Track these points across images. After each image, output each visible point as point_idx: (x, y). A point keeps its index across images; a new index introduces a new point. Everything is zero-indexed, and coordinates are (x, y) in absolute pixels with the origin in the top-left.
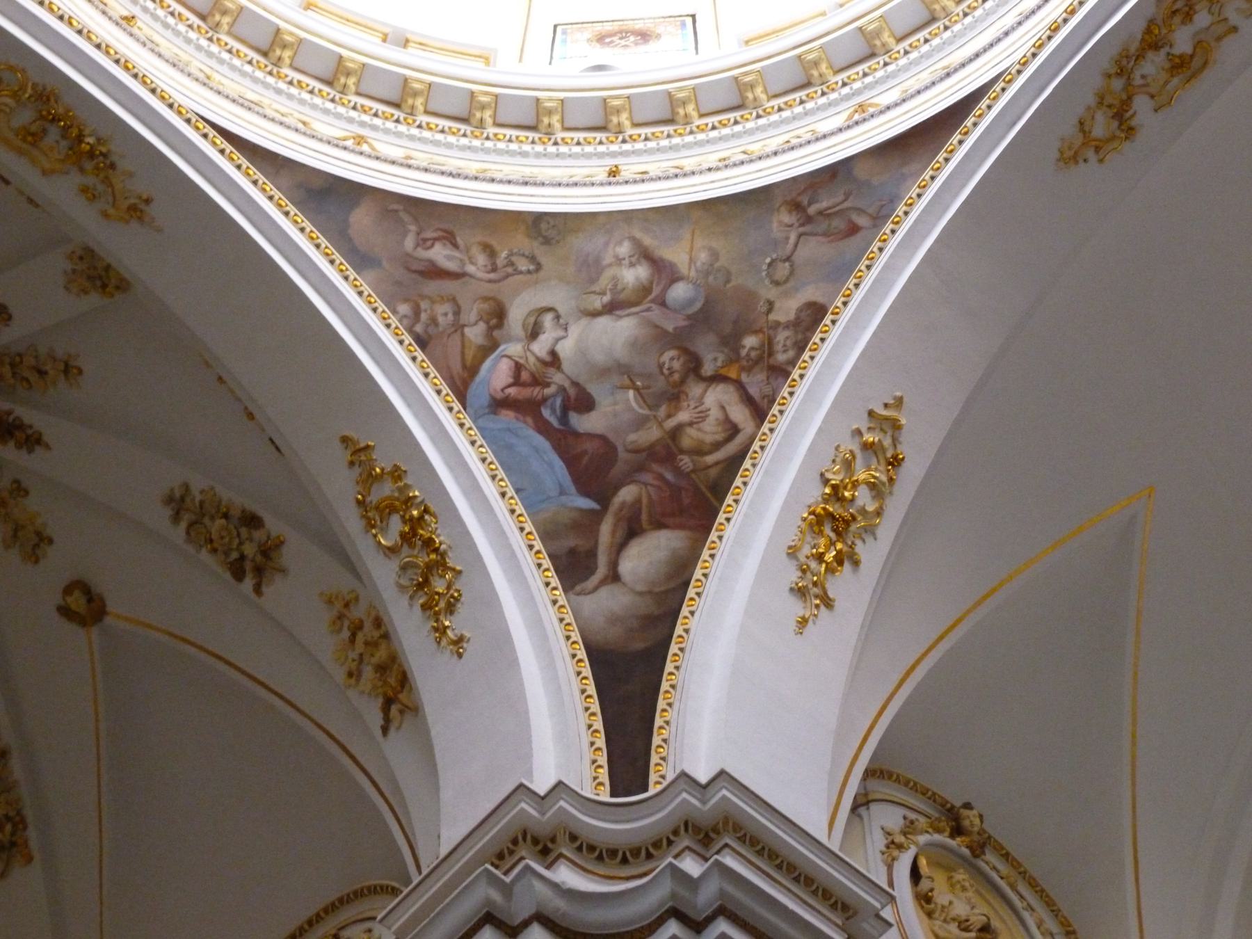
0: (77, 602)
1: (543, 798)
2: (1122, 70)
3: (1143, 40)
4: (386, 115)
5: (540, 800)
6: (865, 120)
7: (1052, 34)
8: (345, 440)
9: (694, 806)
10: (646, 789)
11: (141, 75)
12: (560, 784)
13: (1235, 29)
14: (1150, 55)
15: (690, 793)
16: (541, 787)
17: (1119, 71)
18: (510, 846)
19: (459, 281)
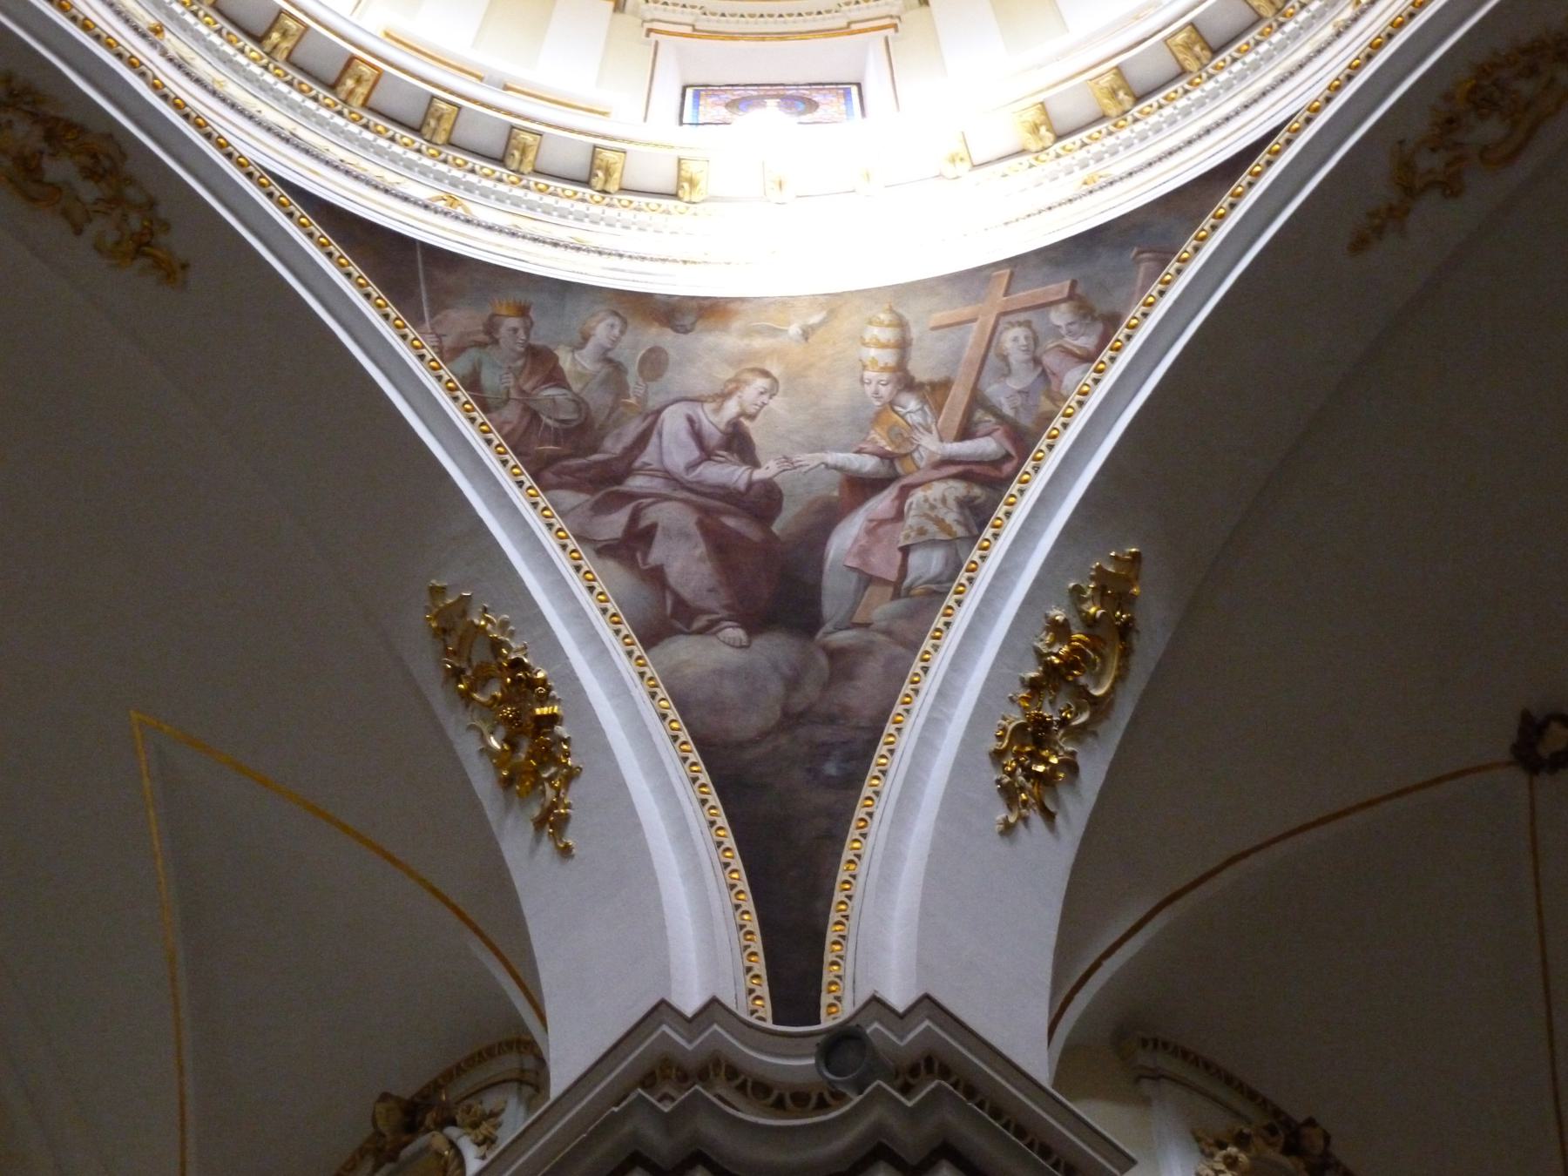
2: (17, 95)
3: (58, 120)
6: (446, 214)
7: (192, 121)
12: (714, 1002)
13: (78, 231)
14: (38, 131)
16: (690, 1003)
17: (16, 92)
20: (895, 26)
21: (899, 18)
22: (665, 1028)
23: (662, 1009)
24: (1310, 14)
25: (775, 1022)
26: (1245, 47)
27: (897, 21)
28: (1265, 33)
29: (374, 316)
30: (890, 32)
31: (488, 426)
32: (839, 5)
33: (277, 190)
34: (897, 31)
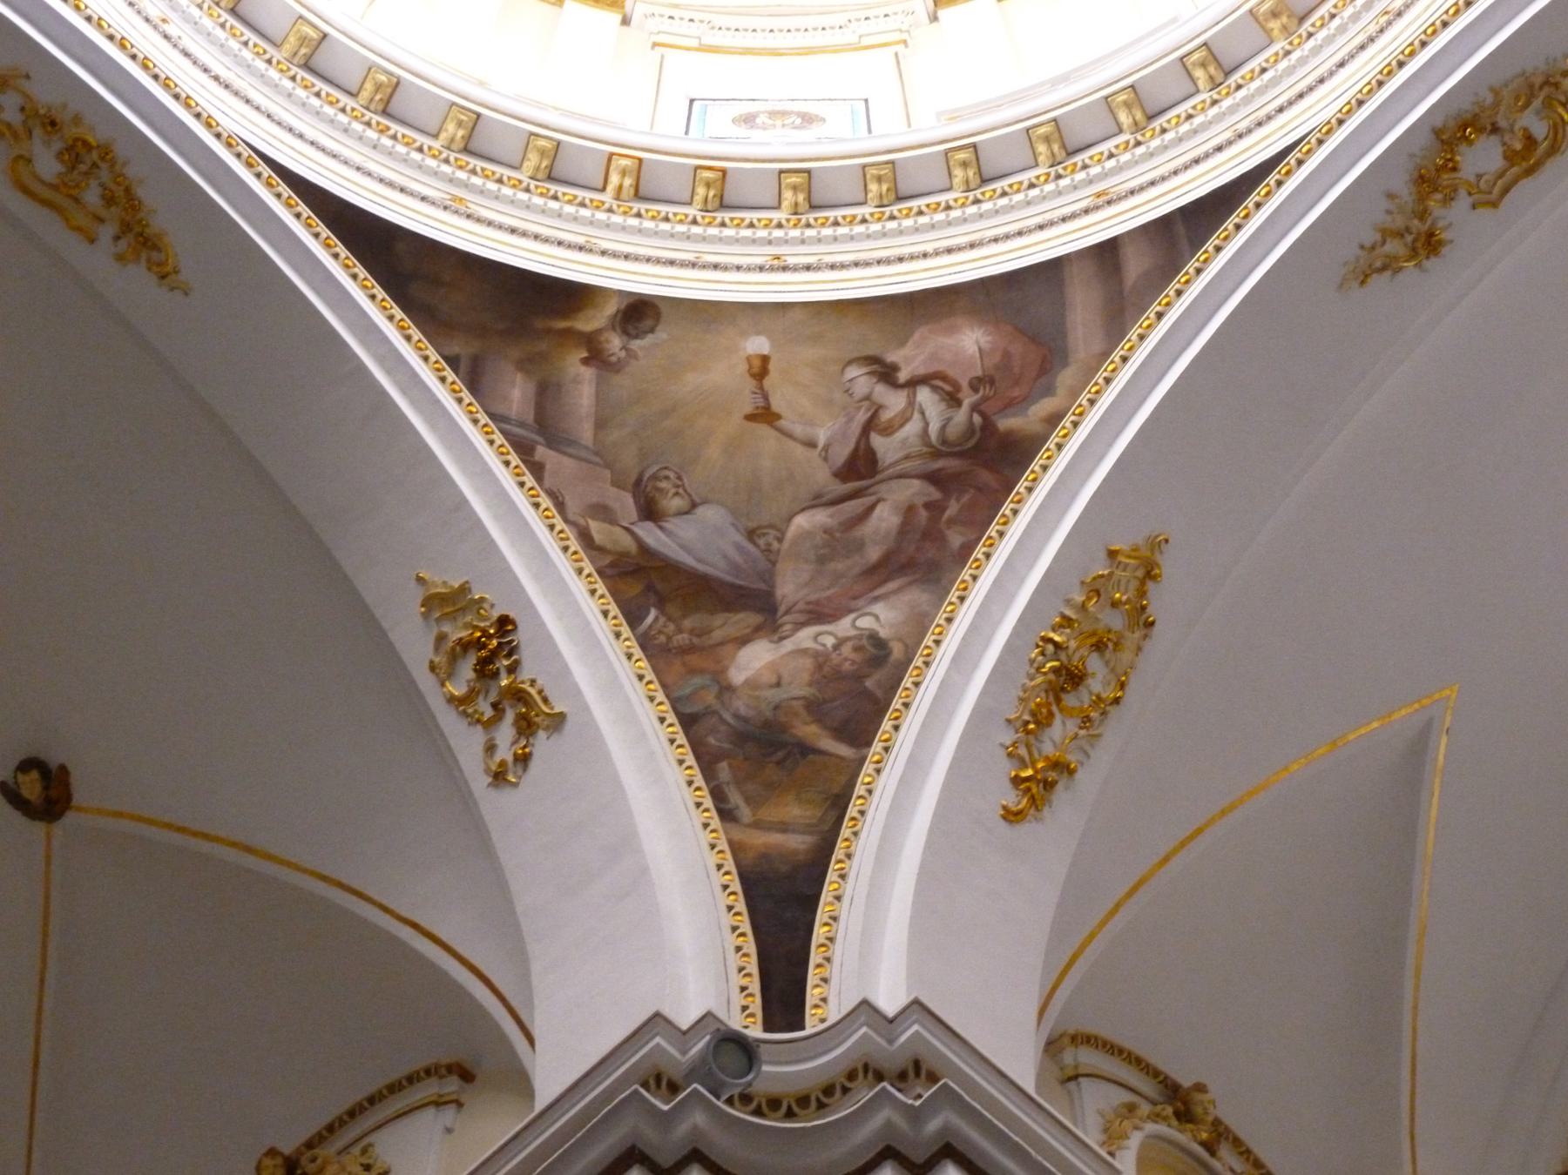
0: (31, 786)
1: (685, 1033)
4: (486, 173)
5: (680, 1034)
8: (420, 580)
9: (671, 1056)
10: (802, 1028)
11: (1423, 37)
15: (924, 1026)
18: (861, 1075)
19: (847, 360)
20: (905, 42)
21: (908, 31)
22: (658, 1040)
23: (657, 1021)
24: (211, 30)
25: (768, 1027)
26: (238, 33)
27: (905, 36)
28: (233, 31)
29: (424, 371)
30: (900, 48)
31: (506, 448)
32: (850, 21)
33: (266, 171)
34: (906, 46)
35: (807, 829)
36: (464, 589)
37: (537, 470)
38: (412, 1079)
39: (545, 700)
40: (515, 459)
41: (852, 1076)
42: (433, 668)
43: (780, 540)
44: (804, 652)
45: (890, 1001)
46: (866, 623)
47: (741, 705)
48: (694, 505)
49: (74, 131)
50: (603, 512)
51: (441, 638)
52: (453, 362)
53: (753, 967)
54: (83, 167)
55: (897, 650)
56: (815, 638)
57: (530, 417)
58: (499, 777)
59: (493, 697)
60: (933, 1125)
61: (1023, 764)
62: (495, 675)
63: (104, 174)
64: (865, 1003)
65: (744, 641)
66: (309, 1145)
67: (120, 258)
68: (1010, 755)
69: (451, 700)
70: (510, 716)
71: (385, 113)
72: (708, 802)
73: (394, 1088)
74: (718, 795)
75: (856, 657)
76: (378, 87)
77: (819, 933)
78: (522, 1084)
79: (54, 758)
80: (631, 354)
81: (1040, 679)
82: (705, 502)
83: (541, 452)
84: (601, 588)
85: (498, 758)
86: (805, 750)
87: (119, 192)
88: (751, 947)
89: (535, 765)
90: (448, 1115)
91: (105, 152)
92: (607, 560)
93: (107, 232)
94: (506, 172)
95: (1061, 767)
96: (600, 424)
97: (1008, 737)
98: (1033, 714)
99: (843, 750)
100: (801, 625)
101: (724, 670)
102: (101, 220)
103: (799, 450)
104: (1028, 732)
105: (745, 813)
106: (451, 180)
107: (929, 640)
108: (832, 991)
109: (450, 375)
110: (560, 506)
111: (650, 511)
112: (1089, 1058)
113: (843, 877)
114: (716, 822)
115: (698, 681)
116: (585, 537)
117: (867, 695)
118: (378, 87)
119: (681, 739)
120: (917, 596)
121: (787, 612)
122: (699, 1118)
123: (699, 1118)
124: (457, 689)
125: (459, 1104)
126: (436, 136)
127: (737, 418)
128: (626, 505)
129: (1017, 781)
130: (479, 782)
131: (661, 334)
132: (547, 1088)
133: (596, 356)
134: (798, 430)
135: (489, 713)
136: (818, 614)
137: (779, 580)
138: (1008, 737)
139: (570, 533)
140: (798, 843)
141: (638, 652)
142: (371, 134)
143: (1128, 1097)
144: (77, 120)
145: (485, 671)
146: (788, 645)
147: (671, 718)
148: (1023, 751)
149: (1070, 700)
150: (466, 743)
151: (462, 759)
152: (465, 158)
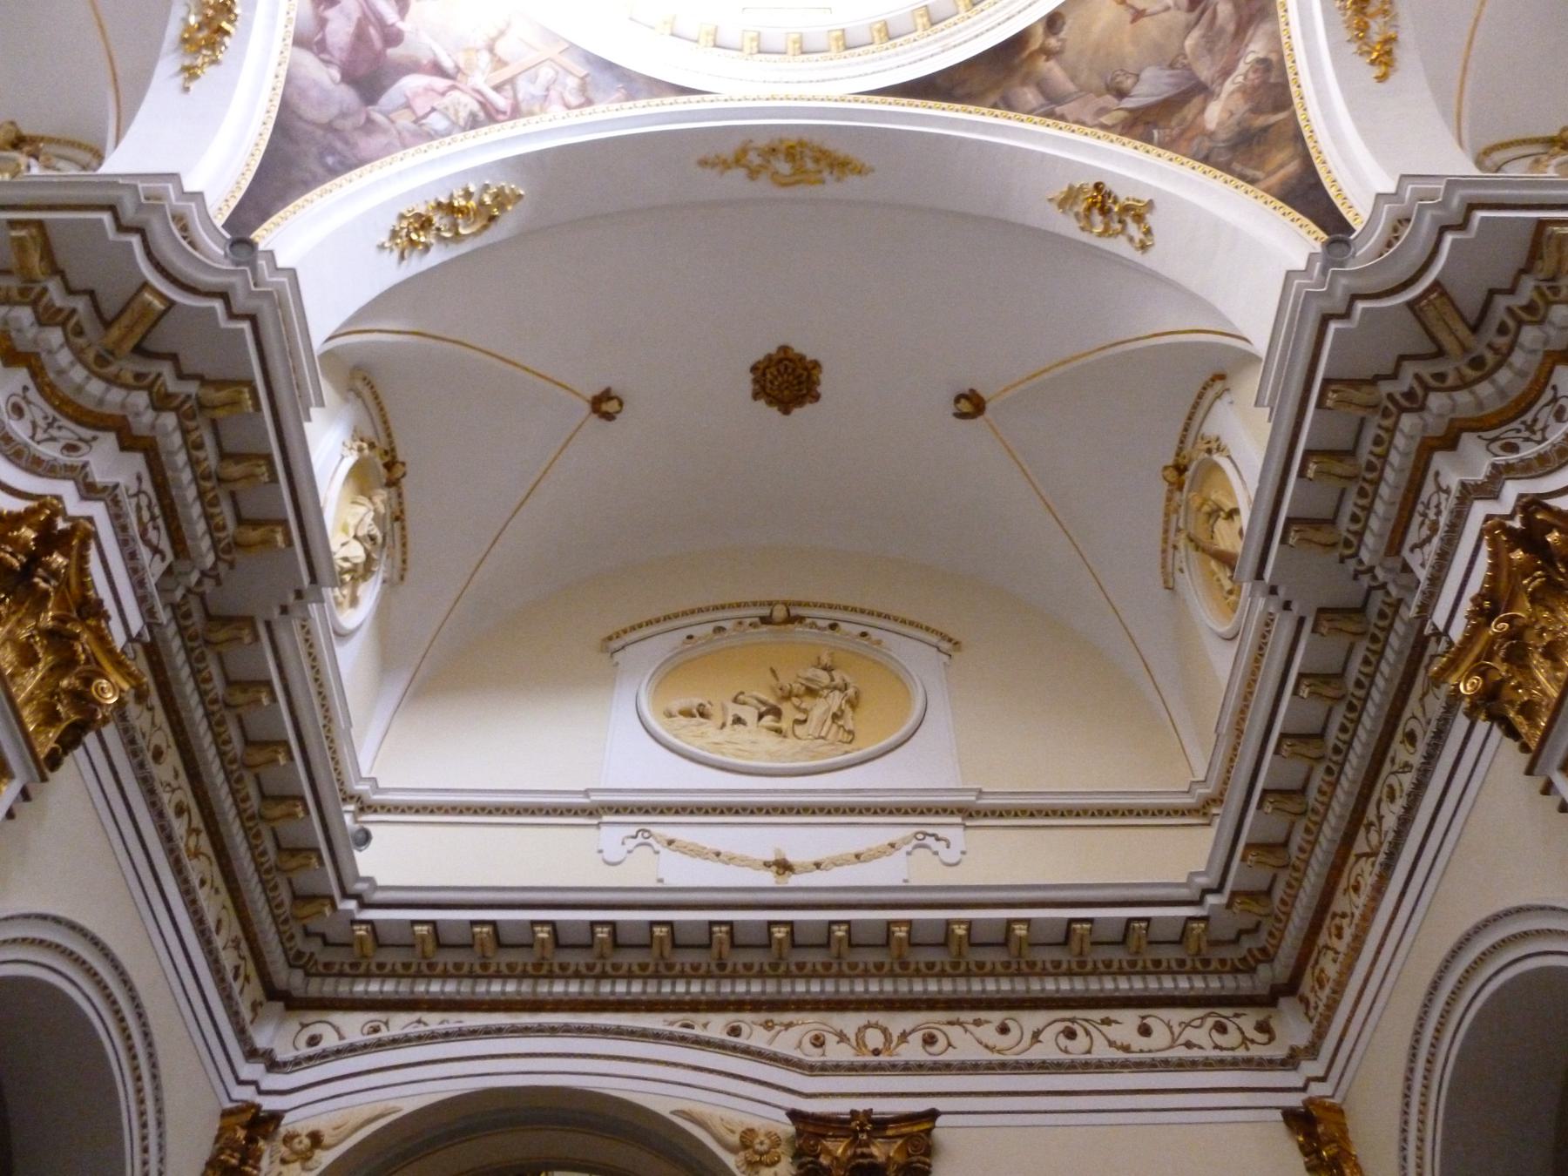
0: (965, 406)
8: (1051, 200)
33: (864, 97)
35: (1292, 158)
36: (1071, 188)
37: (1062, 118)
38: (1200, 396)
39: (1139, 201)
40: (1050, 121)
41: (1395, 230)
42: (1083, 229)
43: (1185, 58)
44: (1232, 93)
45: (1390, 187)
46: (1250, 58)
47: (1223, 135)
48: (1137, 76)
49: (783, 147)
50: (1103, 111)
51: (1077, 215)
52: (995, 106)
53: (1313, 227)
54: (798, 157)
55: (1274, 57)
56: (1233, 83)
57: (1042, 100)
58: (1144, 247)
59: (1116, 218)
60: (1455, 202)
61: (1370, 53)
62: (1110, 210)
63: (807, 152)
64: (1379, 196)
65: (1202, 110)
66: (1178, 455)
67: (839, 180)
68: (1361, 54)
69: (1100, 235)
70: (1129, 220)
71: (890, 39)
72: (1240, 183)
73: (1195, 406)
74: (1242, 177)
75: (1258, 75)
76: (879, 31)
77: (1332, 192)
78: (1249, 359)
79: (965, 389)
80: (1064, 41)
81: (1349, 13)
82: (1141, 70)
83: (1059, 110)
84: (1126, 140)
85: (1137, 240)
86: (1265, 129)
87: (818, 155)
88: (1306, 221)
89: (1155, 230)
90: (1226, 398)
91: (801, 143)
92: (1119, 129)
93: (826, 174)
94: (955, 19)
95: (1389, 40)
96: (1073, 79)
97: (1354, 47)
98: (1358, 29)
99: (1281, 116)
100: (1222, 84)
101: (1204, 128)
102: (820, 172)
103: (1165, 16)
104: (1361, 38)
105: (1259, 174)
106: (936, 41)
107: (1284, 40)
108: (1358, 209)
109: (998, 112)
110: (1083, 123)
111: (1121, 94)
112: (1498, 157)
113: (1324, 162)
114: (1250, 188)
115: (1196, 141)
116: (1104, 127)
117: (1275, 85)
118: (879, 31)
119: (1208, 168)
120: (1266, 27)
121: (1213, 83)
122: (1343, 281)
123: (1343, 281)
124: (1099, 229)
125: (1228, 390)
126: (916, 30)
127: (1129, 27)
128: (1109, 100)
129: (1373, 62)
130: (1137, 256)
131: (1069, 22)
132: (1260, 346)
133: (1049, 53)
134: (1157, 7)
135: (1118, 226)
136: (1226, 73)
137: (1198, 74)
138: (1354, 47)
139: (1095, 130)
140: (1293, 167)
141: (1161, 151)
142: (891, 51)
143: (1532, 158)
144: (781, 141)
145: (1105, 211)
146: (1224, 95)
147: (1197, 164)
148: (1366, 48)
149: (1371, 10)
150: (1120, 246)
151: (1125, 255)
152: (934, 28)
